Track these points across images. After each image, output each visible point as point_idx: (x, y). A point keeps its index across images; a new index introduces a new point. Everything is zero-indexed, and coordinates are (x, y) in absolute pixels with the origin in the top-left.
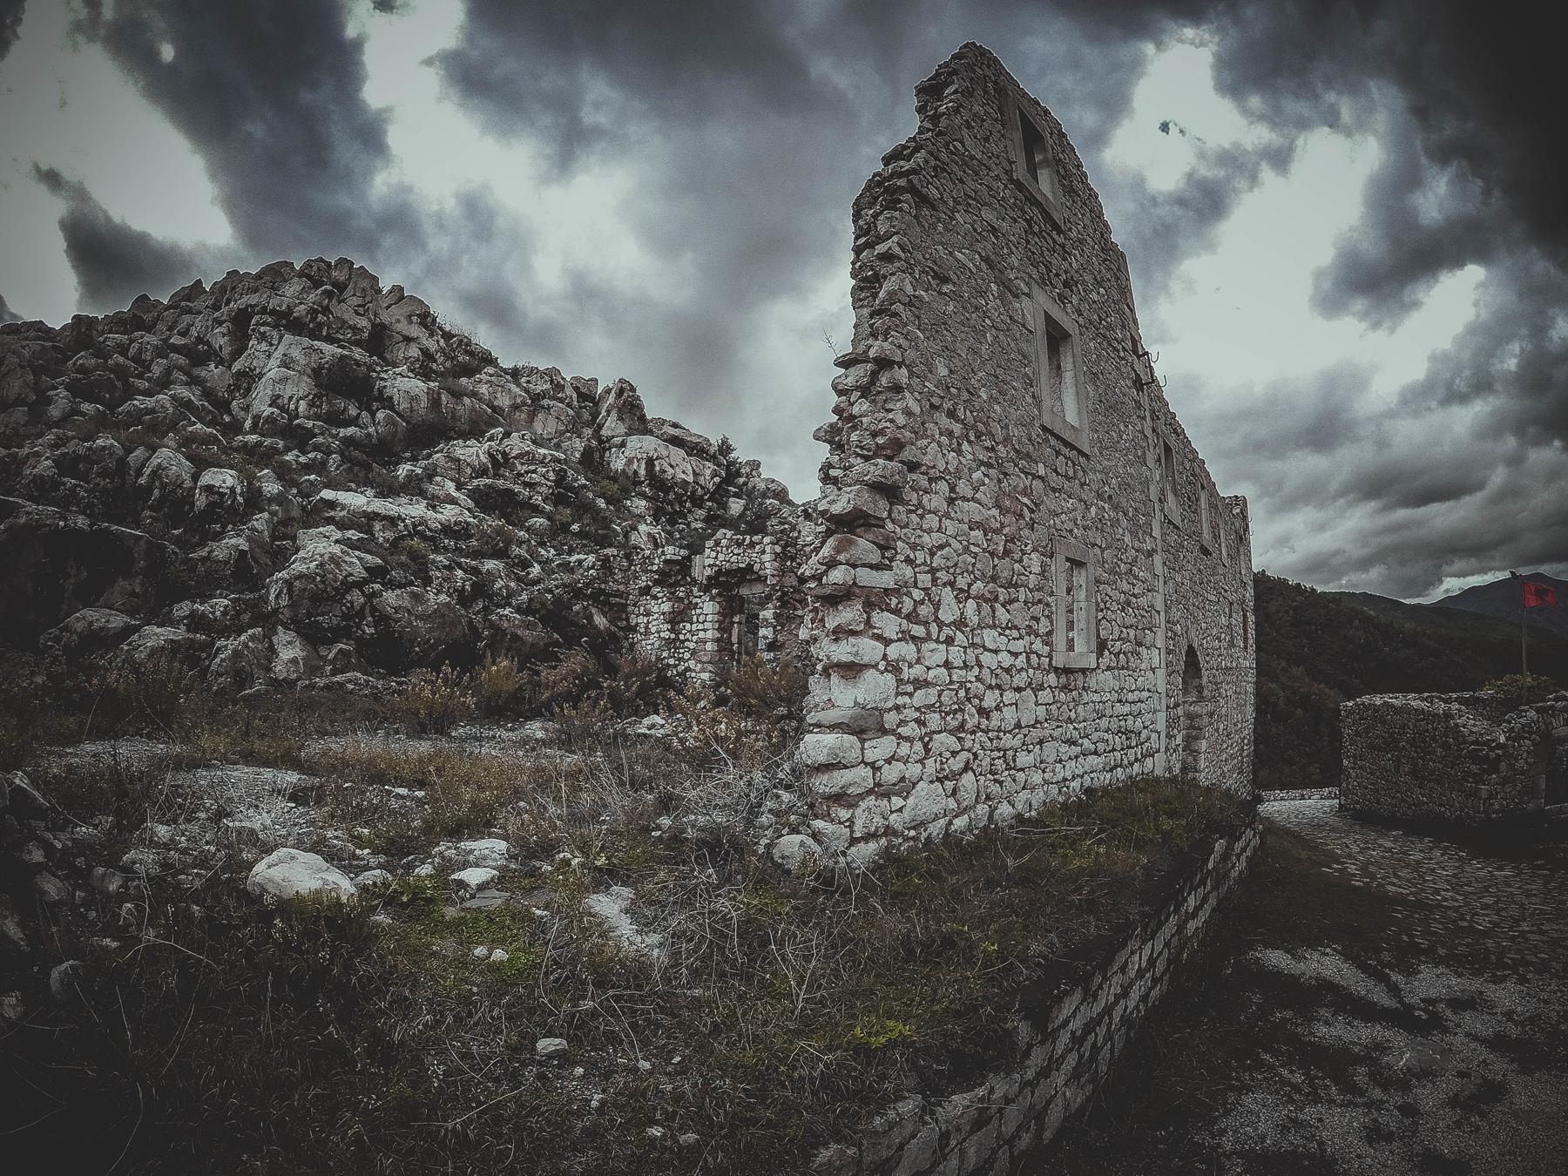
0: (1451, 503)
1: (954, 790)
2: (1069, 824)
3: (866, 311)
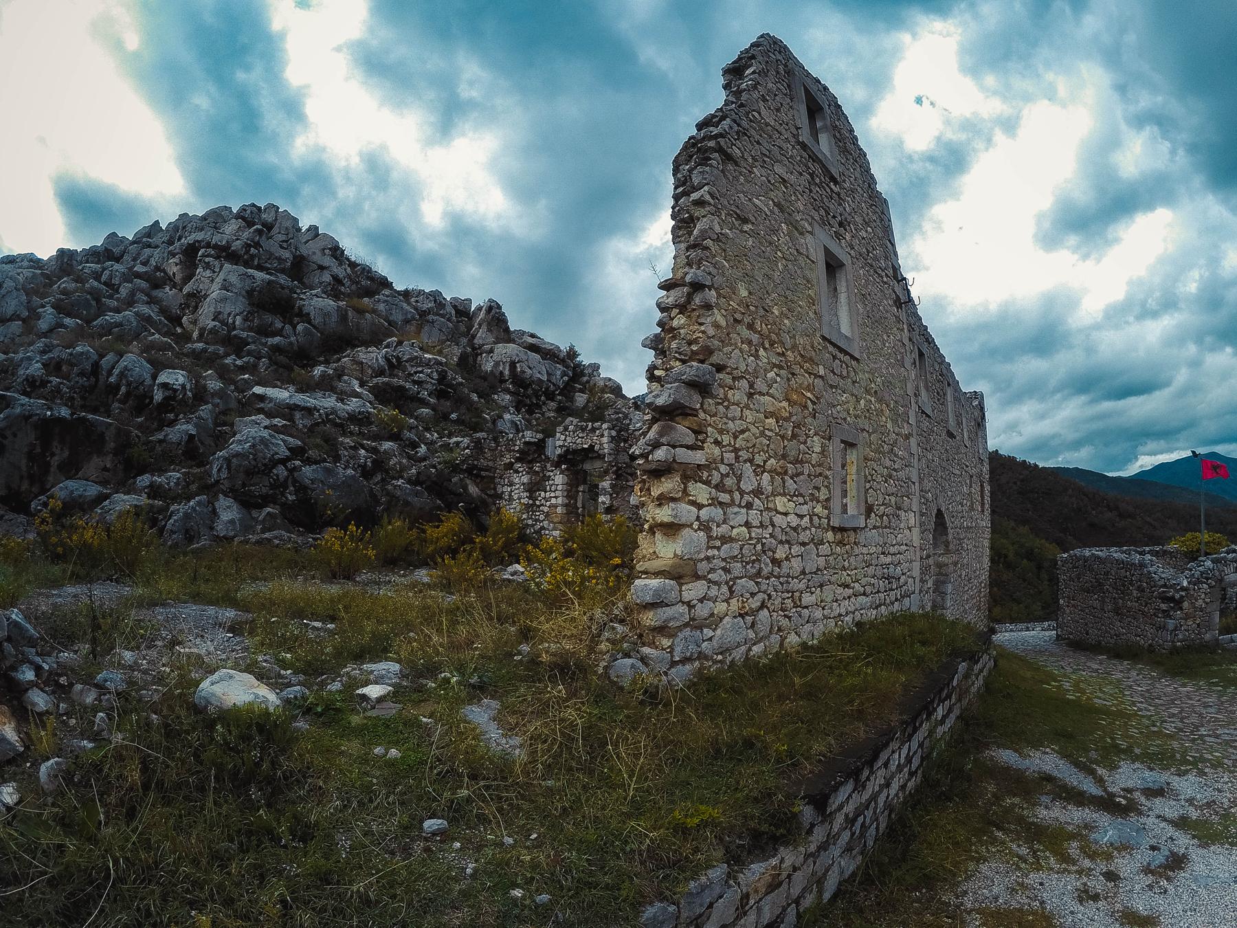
1: (753, 623)
2: (843, 650)
3: (683, 246)
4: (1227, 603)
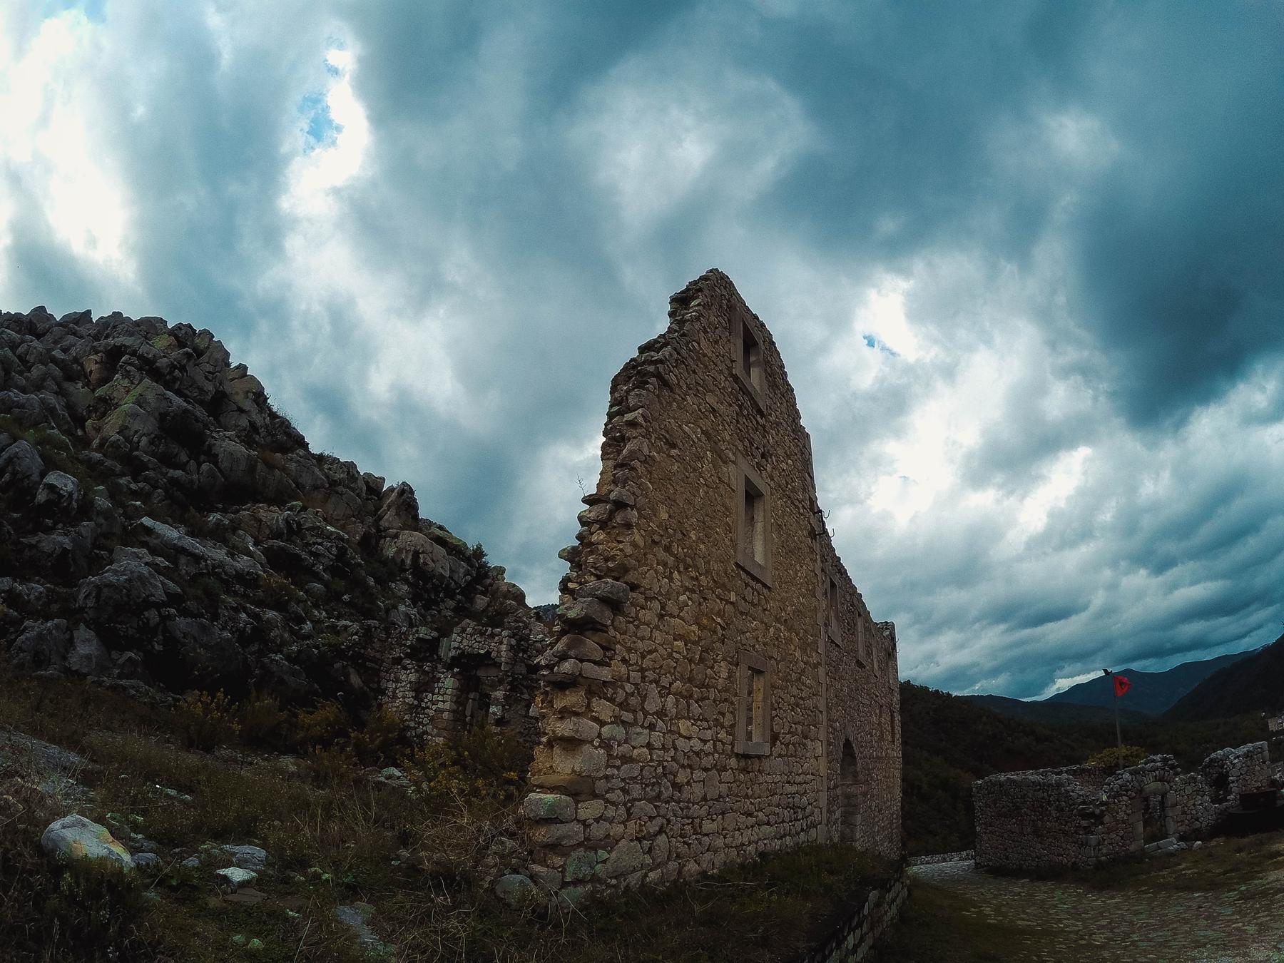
0: (1062, 621)
1: (650, 848)
2: (745, 880)
3: (610, 463)
4: (1151, 813)
